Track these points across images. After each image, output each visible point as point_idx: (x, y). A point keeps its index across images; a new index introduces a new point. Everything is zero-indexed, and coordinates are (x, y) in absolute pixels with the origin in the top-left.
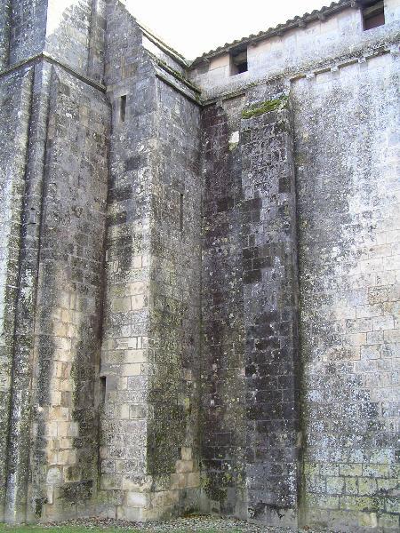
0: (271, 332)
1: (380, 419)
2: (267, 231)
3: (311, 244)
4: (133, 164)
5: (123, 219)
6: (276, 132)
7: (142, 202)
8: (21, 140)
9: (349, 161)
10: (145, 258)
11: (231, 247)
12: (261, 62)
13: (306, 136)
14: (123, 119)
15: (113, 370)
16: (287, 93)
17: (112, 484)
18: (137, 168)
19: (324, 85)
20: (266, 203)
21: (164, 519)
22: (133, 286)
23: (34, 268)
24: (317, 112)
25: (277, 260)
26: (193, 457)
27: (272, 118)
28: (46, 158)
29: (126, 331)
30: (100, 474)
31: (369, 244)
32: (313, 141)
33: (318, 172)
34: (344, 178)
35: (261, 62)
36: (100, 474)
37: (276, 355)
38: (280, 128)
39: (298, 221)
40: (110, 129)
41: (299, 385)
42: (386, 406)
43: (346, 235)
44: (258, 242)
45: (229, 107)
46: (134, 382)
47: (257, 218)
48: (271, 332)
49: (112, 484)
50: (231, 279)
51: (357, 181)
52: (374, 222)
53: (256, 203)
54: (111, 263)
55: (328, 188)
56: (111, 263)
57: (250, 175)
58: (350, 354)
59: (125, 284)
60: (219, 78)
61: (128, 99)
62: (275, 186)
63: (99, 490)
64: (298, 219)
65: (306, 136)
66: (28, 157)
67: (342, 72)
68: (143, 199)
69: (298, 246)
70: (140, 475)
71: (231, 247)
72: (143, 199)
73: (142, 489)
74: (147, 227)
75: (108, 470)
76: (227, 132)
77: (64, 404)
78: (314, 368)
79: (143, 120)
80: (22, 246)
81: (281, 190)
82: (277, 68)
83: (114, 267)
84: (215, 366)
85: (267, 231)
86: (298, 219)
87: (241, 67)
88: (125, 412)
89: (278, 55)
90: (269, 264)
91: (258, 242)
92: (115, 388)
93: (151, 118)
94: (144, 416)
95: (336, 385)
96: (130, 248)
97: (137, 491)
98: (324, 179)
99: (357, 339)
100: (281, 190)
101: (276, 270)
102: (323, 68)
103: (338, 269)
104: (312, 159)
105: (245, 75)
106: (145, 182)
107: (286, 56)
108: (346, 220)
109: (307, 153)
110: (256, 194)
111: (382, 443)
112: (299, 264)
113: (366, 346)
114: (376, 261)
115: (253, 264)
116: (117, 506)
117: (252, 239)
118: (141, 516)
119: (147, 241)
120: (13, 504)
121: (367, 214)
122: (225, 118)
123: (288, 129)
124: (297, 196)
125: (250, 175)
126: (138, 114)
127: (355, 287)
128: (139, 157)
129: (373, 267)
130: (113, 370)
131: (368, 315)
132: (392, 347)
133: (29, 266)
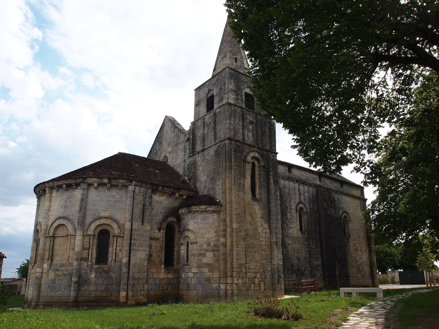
99: (290, 247)
108: (287, 218)
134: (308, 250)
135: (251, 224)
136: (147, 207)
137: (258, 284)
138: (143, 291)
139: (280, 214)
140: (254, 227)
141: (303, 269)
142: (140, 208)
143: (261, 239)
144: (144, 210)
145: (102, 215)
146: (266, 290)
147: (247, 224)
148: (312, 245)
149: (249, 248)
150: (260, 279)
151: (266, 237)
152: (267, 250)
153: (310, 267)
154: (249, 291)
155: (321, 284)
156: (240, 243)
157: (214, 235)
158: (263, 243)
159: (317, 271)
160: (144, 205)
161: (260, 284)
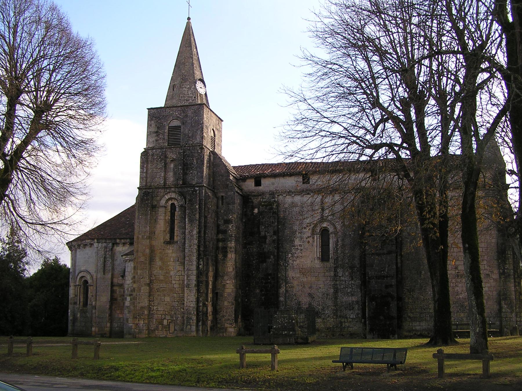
0: (269, 279)
1: (301, 306)
2: (268, 247)
3: (282, 252)
4: (228, 222)
5: (224, 240)
6: (273, 214)
7: (231, 236)
8: (197, 216)
9: (296, 228)
10: (233, 255)
11: (254, 249)
12: (267, 184)
13: (282, 216)
14: (222, 204)
15: (221, 290)
16: (276, 199)
17: (221, 326)
18: (229, 224)
19: (289, 200)
20: (268, 237)
21: (237, 336)
22: (228, 264)
23: (203, 259)
24: (286, 208)
25: (272, 257)
26: (478, 244)
27: (272, 209)
28: (205, 222)
29: (226, 278)
30: (216, 323)
31: (300, 254)
32: (284, 218)
33: (285, 229)
34: (294, 232)
35: (267, 184)
36: (216, 323)
37: (271, 286)
38: (274, 213)
39: (279, 244)
40: (218, 207)
41: (277, 296)
42: (303, 302)
43: (294, 251)
44: (265, 250)
45: (254, 199)
46: (229, 294)
47: (265, 242)
48: (269, 279)
49: (221, 326)
50: (254, 260)
51: (298, 235)
52: (302, 248)
53: (265, 237)
54: (219, 255)
55: (288, 235)
56: (219, 255)
57: (263, 227)
58: (293, 287)
59: (225, 263)
60: (250, 185)
61: (224, 198)
62: (272, 233)
63: (216, 328)
64: (278, 244)
65: (282, 216)
66: (200, 222)
67: (295, 197)
68: (232, 235)
69: (278, 253)
70: (232, 323)
71: (254, 249)
72: (232, 235)
73: (233, 327)
74: (233, 245)
75: (219, 322)
76: (253, 208)
77: (210, 301)
78: (282, 290)
79: (231, 207)
80: (199, 252)
81: (274, 235)
82: (272, 188)
83: (220, 256)
84: (247, 288)
85: (268, 247)
86: (278, 244)
87: (258, 183)
88: (226, 303)
89: (273, 184)
90: (269, 258)
91: (265, 250)
92: (222, 296)
93: (234, 207)
94: (233, 305)
95: (289, 296)
96: (227, 251)
97: (231, 327)
98: (287, 232)
99: (295, 283)
100: (274, 235)
101: (272, 259)
102: (290, 193)
103: (290, 261)
104: (284, 224)
105: (260, 188)
106: (232, 229)
107: (276, 185)
108: (294, 246)
109: (282, 222)
110: (265, 234)
111: (301, 313)
112: (278, 258)
113: (298, 285)
114: (302, 260)
115: (263, 257)
116: (223, 332)
117: (263, 248)
118: (233, 334)
119: (233, 250)
120: (200, 331)
121: (300, 245)
122: (252, 202)
123: (276, 213)
124: (278, 236)
125: (263, 227)
126: (229, 204)
127: (295, 267)
128: (229, 220)
129: (301, 262)
130: (221, 290)
131: (299, 276)
132: (305, 286)
133: (202, 258)
134: (333, 283)
135: (161, 268)
136: (108, 259)
137: (168, 325)
138: (106, 327)
139: (195, 254)
140: (166, 271)
141: (320, 308)
142: (102, 261)
143: (174, 282)
144: (105, 262)
145: (82, 269)
146: (176, 330)
147: (157, 269)
148: (342, 276)
149: (158, 291)
150: (169, 321)
151: (180, 280)
152: (181, 292)
153: (335, 306)
154: (156, 331)
155: (356, 327)
156: (142, 288)
157: (131, 281)
158: (176, 286)
159: (350, 310)
160: (105, 258)
161: (169, 325)
